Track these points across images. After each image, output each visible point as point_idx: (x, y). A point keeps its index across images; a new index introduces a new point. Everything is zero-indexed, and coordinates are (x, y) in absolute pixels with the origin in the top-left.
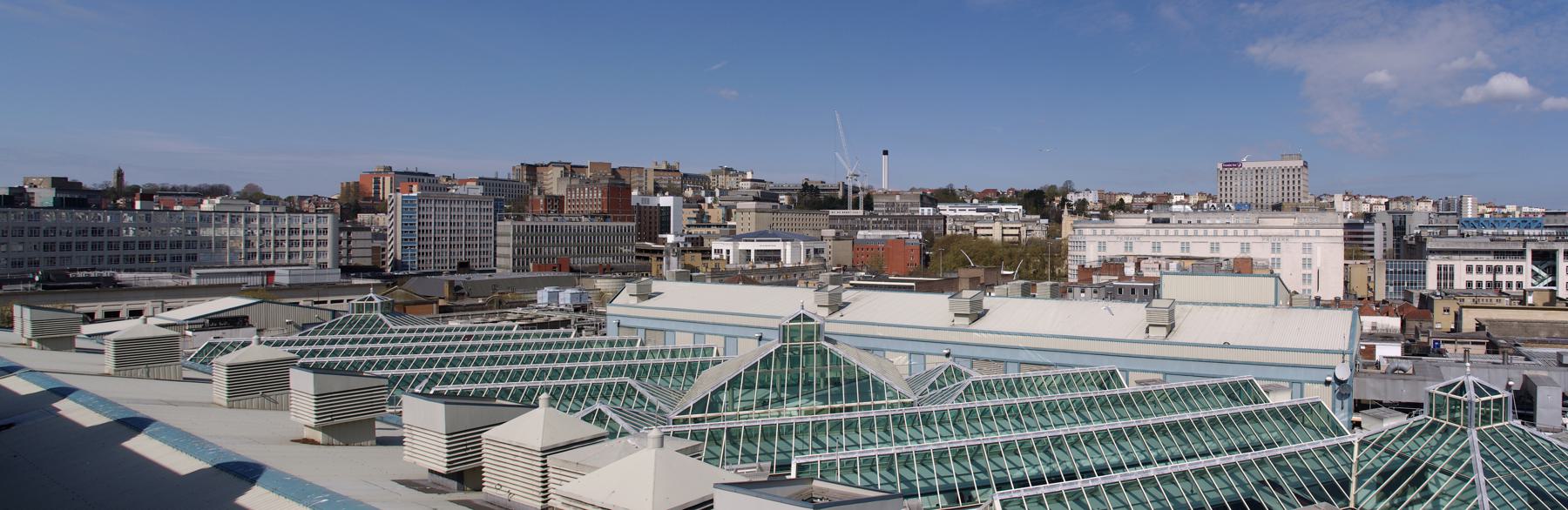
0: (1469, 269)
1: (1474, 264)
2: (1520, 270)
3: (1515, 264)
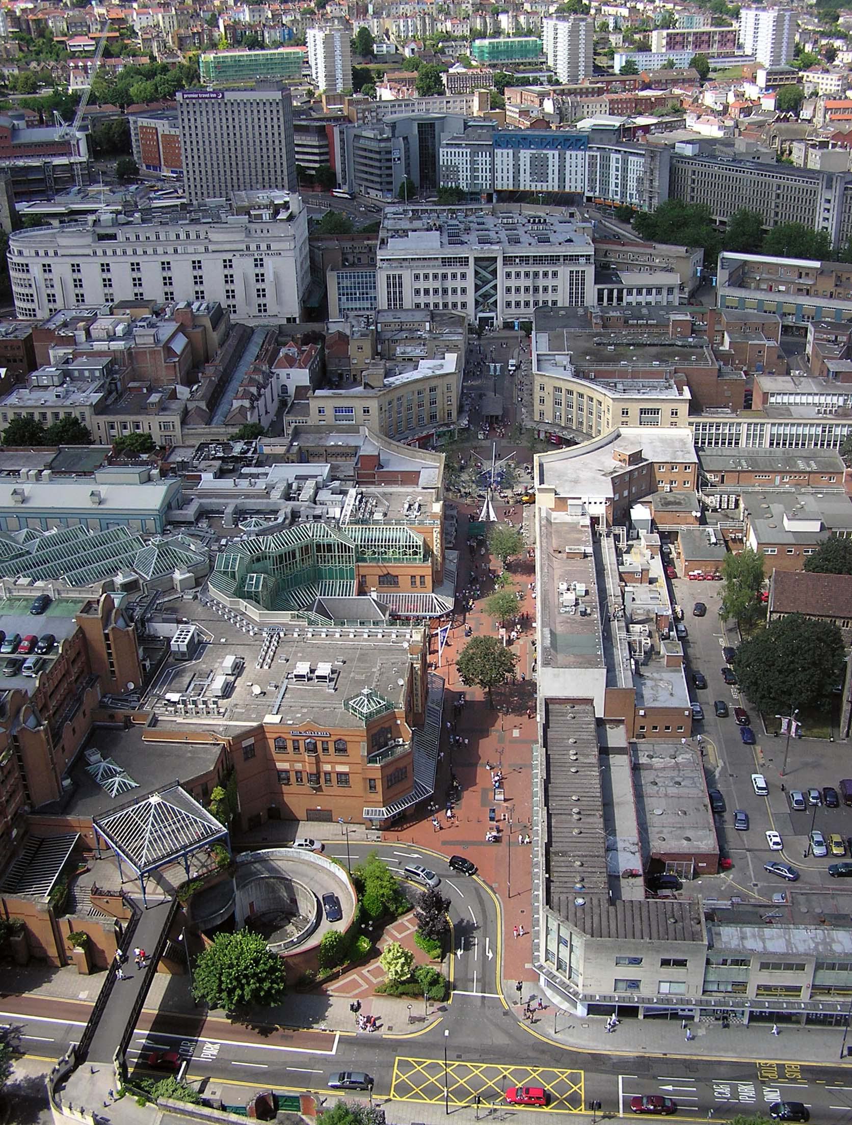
0: (417, 277)
1: (422, 273)
2: (463, 276)
3: (459, 271)
